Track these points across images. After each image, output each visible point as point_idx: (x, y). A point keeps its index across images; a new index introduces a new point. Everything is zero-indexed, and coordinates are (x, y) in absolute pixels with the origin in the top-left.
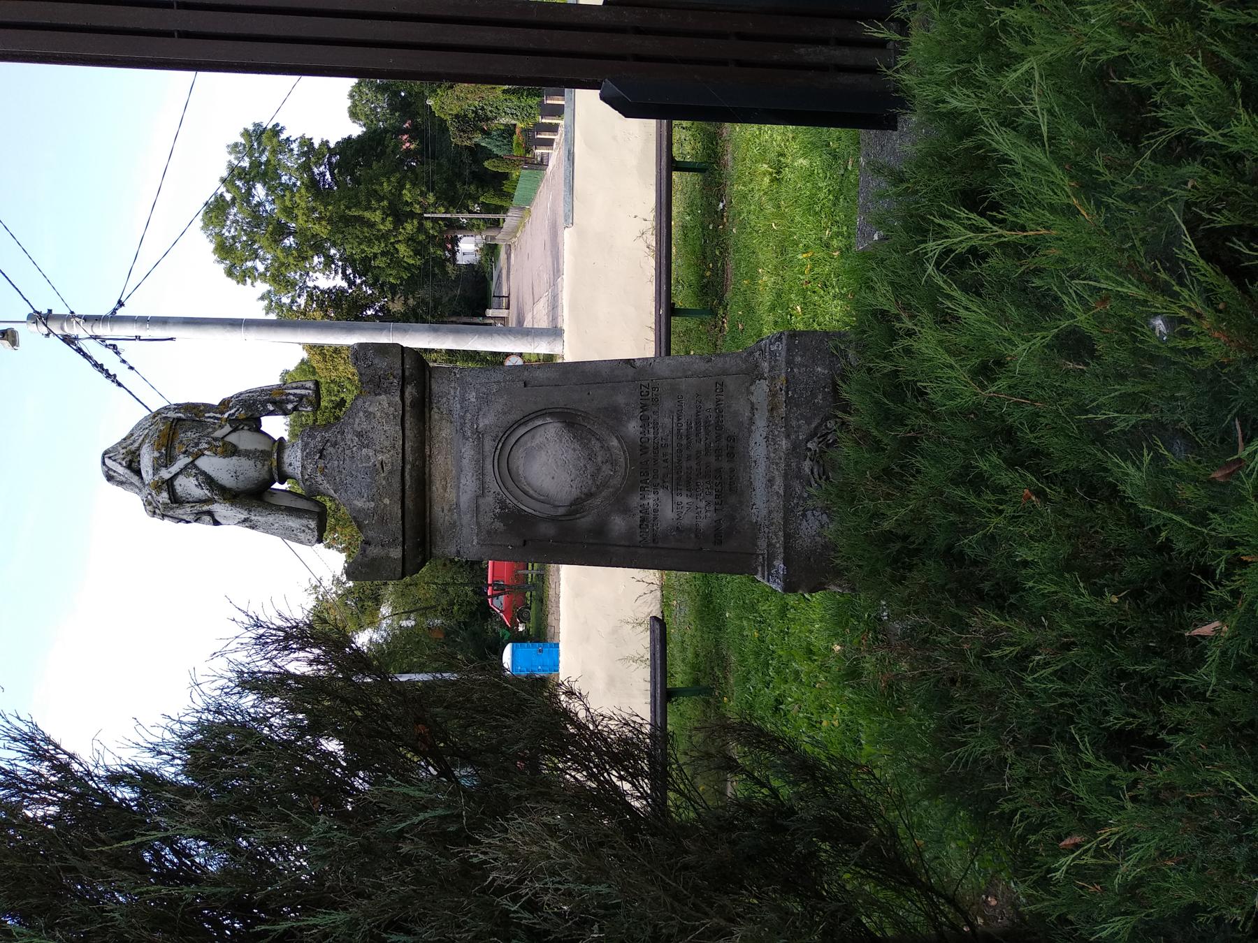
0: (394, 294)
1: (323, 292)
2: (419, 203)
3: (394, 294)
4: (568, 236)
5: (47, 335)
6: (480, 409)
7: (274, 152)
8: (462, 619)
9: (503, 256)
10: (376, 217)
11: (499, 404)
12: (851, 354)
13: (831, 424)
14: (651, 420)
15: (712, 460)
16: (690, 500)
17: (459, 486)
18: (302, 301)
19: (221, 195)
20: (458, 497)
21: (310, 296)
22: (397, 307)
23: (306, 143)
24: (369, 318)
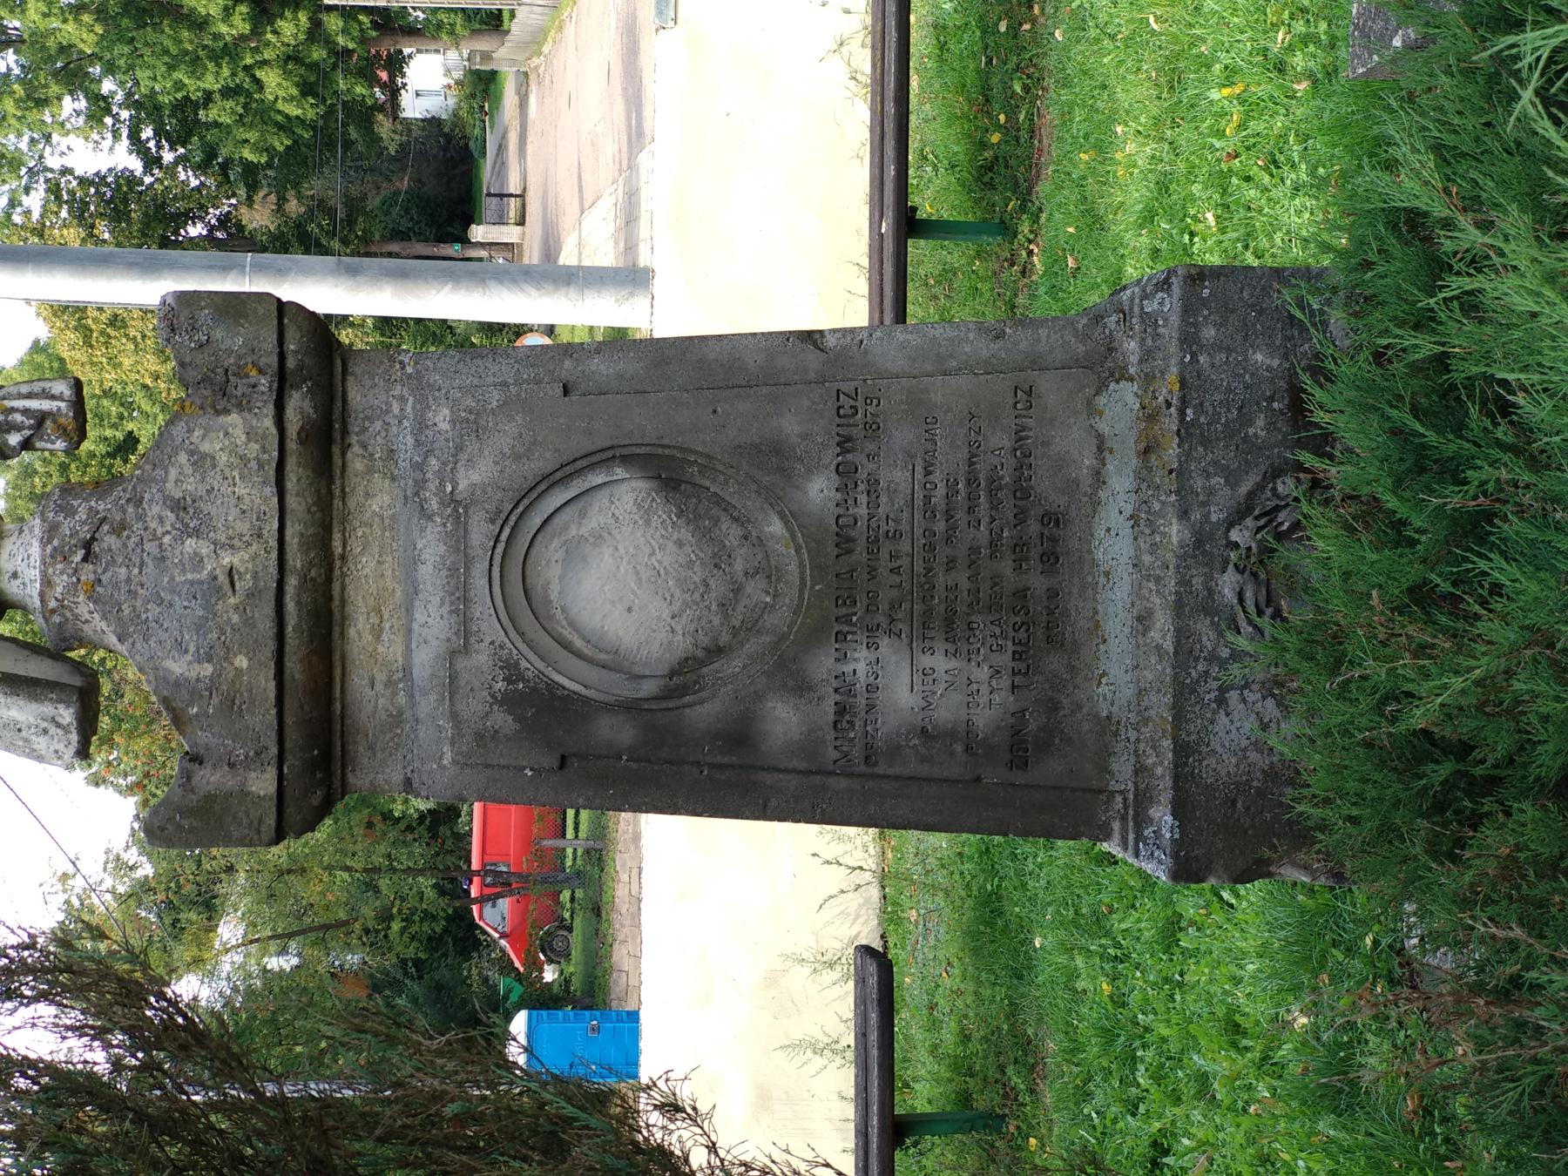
0: (252, 187)
1: (84, 182)
3: (252, 187)
4: (658, 49)
6: (460, 448)
8: (410, 953)
11: (506, 434)
12: (1337, 318)
13: (1286, 486)
14: (862, 475)
15: (1002, 566)
16: (953, 664)
17: (409, 628)
18: (34, 201)
20: (408, 652)
21: (54, 190)
22: (259, 218)
24: (193, 244)
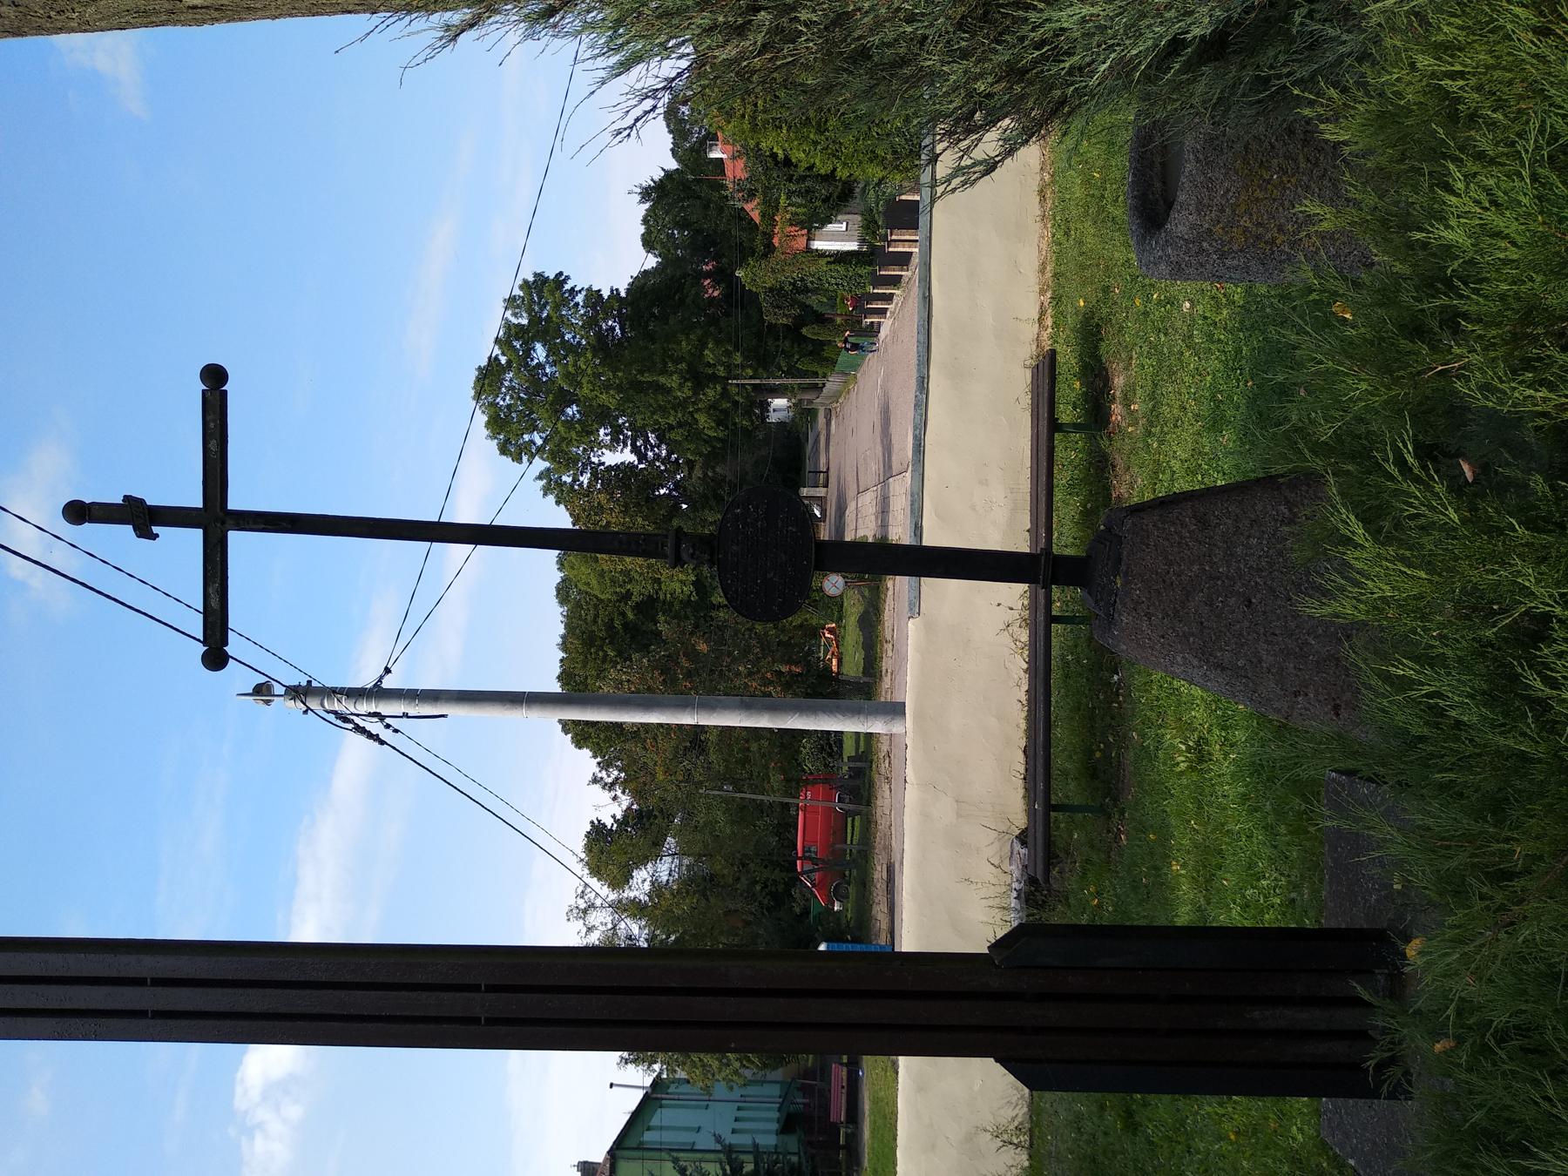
1: (610, 468)
2: (723, 364)
5: (305, 712)
7: (557, 308)
9: (821, 419)
10: (673, 382)
18: (585, 479)
19: (496, 358)
21: (595, 475)
23: (594, 296)
